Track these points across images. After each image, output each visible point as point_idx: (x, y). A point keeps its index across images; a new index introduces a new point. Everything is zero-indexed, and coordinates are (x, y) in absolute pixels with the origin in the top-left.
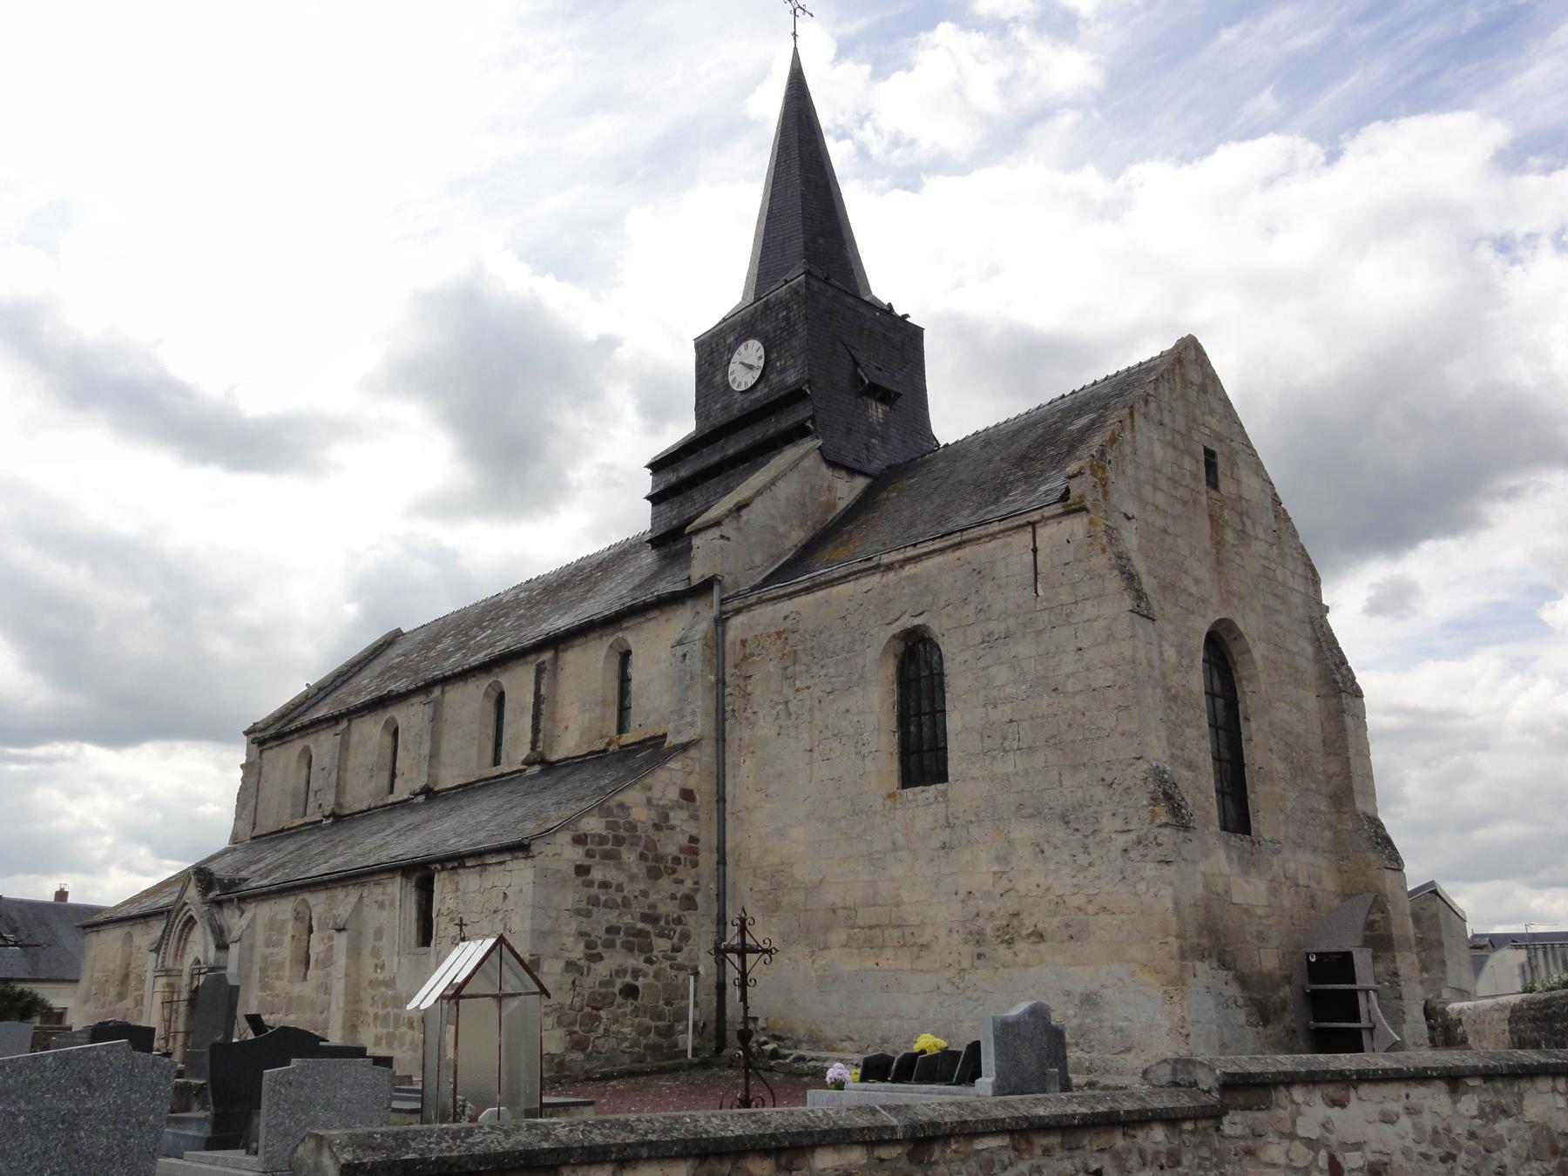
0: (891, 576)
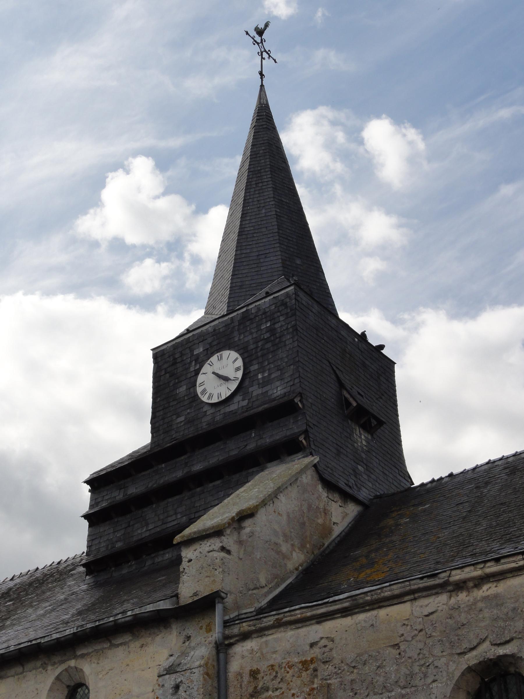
0: (462, 597)
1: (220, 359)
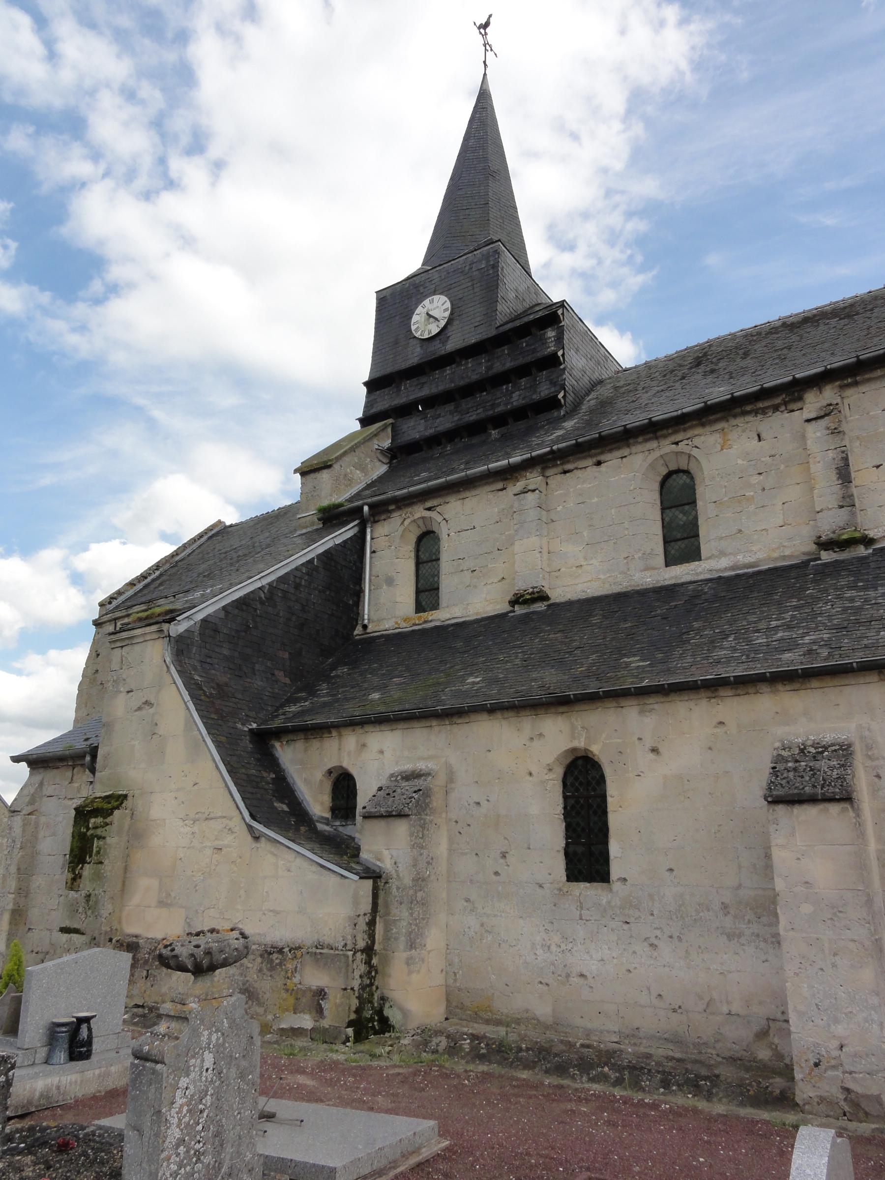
1: (432, 302)
